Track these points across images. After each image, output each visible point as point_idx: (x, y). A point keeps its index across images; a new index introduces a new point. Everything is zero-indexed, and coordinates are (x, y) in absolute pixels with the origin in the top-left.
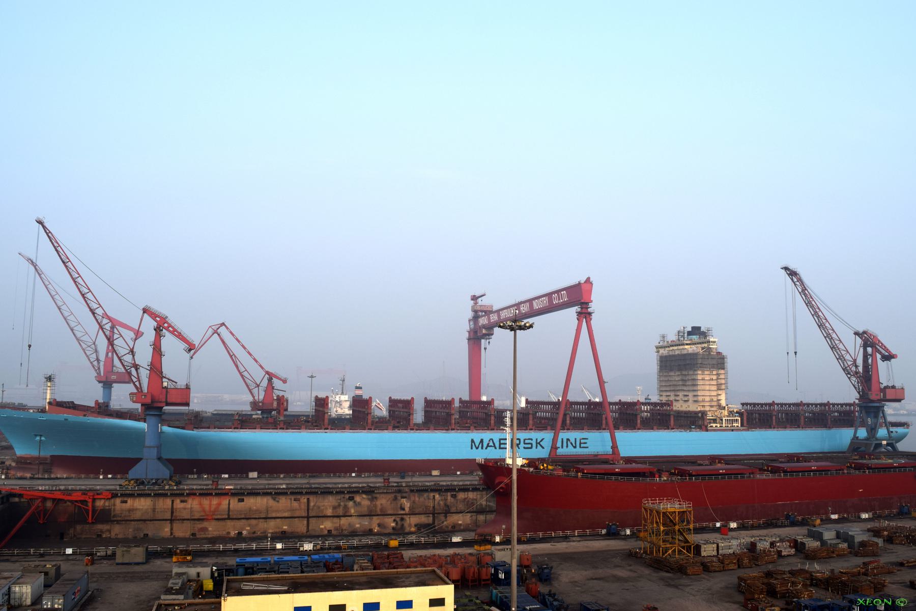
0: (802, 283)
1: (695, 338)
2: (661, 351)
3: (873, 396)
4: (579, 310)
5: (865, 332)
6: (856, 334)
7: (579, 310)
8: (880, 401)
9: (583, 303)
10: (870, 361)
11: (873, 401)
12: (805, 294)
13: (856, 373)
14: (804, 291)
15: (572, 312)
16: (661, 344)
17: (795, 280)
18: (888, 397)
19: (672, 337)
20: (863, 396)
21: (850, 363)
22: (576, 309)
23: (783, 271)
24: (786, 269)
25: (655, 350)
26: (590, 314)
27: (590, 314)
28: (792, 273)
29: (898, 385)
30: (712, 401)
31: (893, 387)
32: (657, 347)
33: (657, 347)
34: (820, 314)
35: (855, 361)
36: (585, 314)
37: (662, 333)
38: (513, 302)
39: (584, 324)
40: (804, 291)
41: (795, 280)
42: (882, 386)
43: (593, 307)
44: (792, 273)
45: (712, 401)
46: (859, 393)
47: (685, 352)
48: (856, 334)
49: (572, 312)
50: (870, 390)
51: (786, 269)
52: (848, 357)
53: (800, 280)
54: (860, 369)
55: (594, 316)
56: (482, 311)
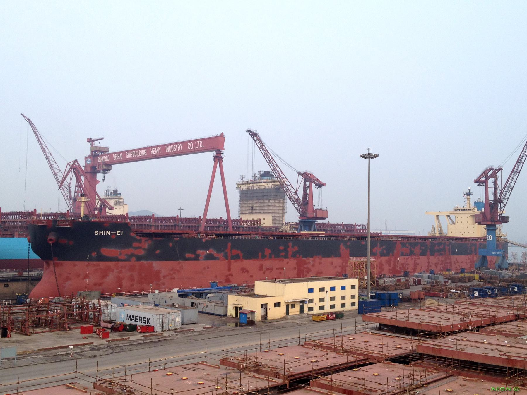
0: (261, 142)
1: (266, 179)
2: (242, 187)
3: (309, 215)
4: (215, 154)
5: (305, 173)
6: (299, 174)
7: (215, 154)
8: (313, 218)
9: (218, 150)
10: (308, 191)
11: (309, 218)
12: (263, 149)
13: (298, 200)
14: (262, 147)
15: (211, 155)
16: (241, 182)
17: (256, 139)
18: (318, 216)
19: (250, 178)
20: (303, 215)
21: (293, 194)
22: (213, 153)
23: (247, 133)
24: (249, 131)
25: (236, 186)
26: (222, 158)
27: (222, 158)
28: (253, 134)
29: (324, 208)
30: (279, 220)
31: (321, 209)
32: (238, 184)
33: (238, 184)
34: (273, 162)
35: (296, 192)
36: (218, 158)
37: (242, 175)
38: (145, 146)
39: (218, 164)
40: (262, 147)
41: (256, 139)
42: (315, 208)
43: (224, 153)
44: (253, 134)
45: (279, 220)
46: (299, 213)
47: (263, 187)
48: (299, 174)
49: (211, 155)
50: (307, 210)
51: (249, 131)
52: (292, 190)
53: (259, 139)
54: (301, 197)
55: (224, 159)
56: (100, 151)
